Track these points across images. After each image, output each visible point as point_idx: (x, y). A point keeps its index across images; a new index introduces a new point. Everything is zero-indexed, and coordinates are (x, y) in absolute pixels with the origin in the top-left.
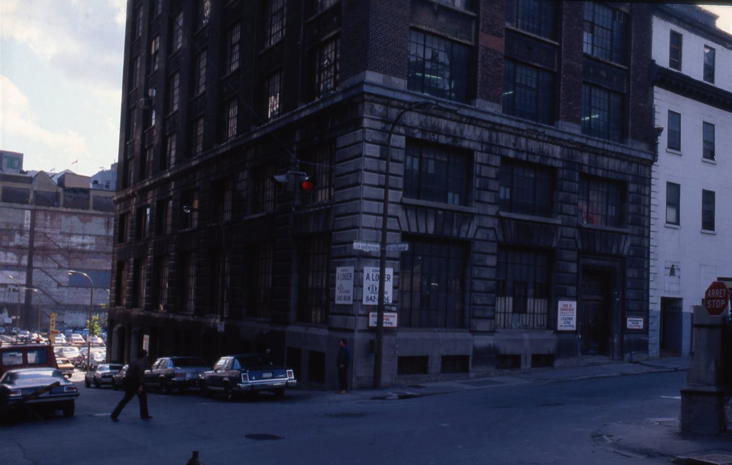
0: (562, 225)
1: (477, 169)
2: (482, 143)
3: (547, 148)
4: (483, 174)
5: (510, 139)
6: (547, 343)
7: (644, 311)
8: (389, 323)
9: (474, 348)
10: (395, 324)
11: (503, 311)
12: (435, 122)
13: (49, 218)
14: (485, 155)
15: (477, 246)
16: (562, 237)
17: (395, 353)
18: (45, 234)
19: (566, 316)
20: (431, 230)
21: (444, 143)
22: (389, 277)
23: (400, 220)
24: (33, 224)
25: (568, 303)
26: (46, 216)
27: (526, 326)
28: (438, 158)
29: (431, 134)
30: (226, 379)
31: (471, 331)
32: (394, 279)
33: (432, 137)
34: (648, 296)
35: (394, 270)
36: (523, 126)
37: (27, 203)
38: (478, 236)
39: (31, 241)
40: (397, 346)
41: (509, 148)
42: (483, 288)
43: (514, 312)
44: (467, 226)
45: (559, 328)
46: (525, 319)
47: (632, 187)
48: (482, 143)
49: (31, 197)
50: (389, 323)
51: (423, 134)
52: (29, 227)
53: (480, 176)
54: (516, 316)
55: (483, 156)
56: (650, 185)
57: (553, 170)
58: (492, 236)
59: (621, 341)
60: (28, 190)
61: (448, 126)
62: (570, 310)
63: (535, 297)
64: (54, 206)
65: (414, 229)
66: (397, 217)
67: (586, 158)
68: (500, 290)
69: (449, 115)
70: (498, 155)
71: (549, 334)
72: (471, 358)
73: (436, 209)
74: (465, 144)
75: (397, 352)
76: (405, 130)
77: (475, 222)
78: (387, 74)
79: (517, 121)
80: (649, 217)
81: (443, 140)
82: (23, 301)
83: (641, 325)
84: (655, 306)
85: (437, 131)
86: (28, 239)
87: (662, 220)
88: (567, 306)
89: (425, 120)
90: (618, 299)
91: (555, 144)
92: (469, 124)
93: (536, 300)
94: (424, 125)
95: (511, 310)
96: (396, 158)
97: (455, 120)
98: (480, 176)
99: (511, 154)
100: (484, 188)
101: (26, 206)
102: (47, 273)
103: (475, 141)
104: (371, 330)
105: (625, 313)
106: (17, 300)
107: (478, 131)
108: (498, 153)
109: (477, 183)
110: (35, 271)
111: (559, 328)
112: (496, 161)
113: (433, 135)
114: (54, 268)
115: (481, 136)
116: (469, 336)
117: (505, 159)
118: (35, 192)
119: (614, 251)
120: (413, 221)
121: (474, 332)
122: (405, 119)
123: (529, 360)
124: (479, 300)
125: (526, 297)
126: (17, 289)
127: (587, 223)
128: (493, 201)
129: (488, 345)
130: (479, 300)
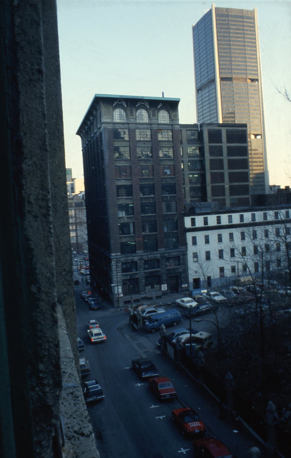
1: (138, 264)
3: (155, 255)
6: (160, 294)
7: (187, 282)
13: (80, 211)
14: (140, 261)
18: (80, 217)
24: (75, 214)
25: (165, 285)
26: (79, 211)
34: (188, 279)
36: (148, 254)
37: (72, 207)
38: (140, 277)
39: (76, 221)
43: (151, 288)
47: (181, 257)
49: (74, 205)
52: (74, 215)
53: (139, 265)
56: (187, 255)
57: (158, 260)
58: (143, 276)
59: (181, 290)
60: (72, 202)
63: (157, 284)
64: (81, 207)
67: (167, 255)
68: (147, 285)
71: (160, 292)
74: (135, 260)
77: (138, 275)
80: (187, 262)
81: (129, 261)
82: (75, 242)
83: (187, 285)
84: (191, 280)
85: (128, 260)
86: (74, 220)
87: (192, 262)
99: (146, 259)
100: (140, 267)
101: (73, 208)
102: (82, 231)
104: (117, 298)
105: (182, 283)
106: (78, 229)
107: (138, 257)
109: (138, 267)
110: (78, 231)
112: (143, 262)
114: (84, 229)
115: (138, 258)
116: (139, 295)
117: (145, 261)
118: (75, 203)
119: (177, 272)
120: (124, 278)
121: (140, 294)
126: (73, 238)
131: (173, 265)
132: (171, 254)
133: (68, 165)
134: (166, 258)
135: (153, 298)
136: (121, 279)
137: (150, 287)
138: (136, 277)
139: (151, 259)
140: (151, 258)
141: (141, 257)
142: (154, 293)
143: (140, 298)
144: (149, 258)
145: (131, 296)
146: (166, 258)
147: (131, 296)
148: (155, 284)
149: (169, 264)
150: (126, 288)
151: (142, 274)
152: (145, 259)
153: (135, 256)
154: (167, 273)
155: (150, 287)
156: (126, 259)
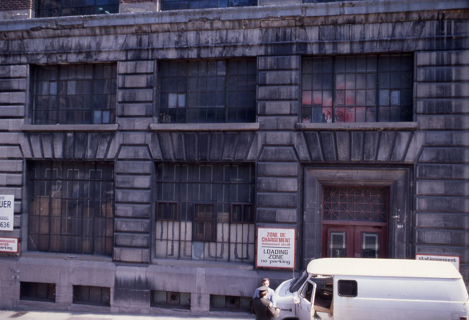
0: (259, 130)
2: (127, 50)
4: (127, 85)
5: (169, 38)
8: (8, 248)
9: (116, 281)
10: (15, 250)
11: (176, 237)
12: (63, 43)
15: (120, 167)
16: (265, 145)
17: (15, 278)
19: (274, 249)
20: (59, 153)
21: (75, 61)
22: (9, 203)
23: (22, 148)
25: (279, 231)
27: (216, 257)
28: (80, 77)
29: (58, 55)
30: (54, 294)
31: (114, 261)
32: (15, 205)
33: (59, 58)
35: (15, 196)
38: (122, 155)
40: (18, 271)
41: (168, 49)
42: (130, 214)
43: (194, 239)
44: (106, 145)
45: (259, 264)
46: (214, 249)
48: (127, 50)
50: (8, 248)
51: (47, 58)
53: (124, 88)
54: (199, 245)
55: (127, 66)
58: (142, 152)
61: (81, 43)
62: (281, 240)
65: (38, 155)
66: (19, 145)
67: (313, 34)
69: (76, 32)
70: (152, 60)
72: (112, 290)
73: (65, 132)
74: (103, 57)
75: (18, 277)
76: (27, 58)
77: (118, 139)
78: (9, 10)
79: (171, 14)
81: (73, 58)
85: (65, 51)
88: (275, 235)
89: (52, 44)
90: (399, 226)
91: (247, 27)
92: (108, 34)
93: (233, 227)
94: (50, 48)
95: (189, 237)
96: (16, 88)
97: (87, 35)
98: (124, 88)
99: (172, 55)
103: (115, 51)
108: (150, 58)
109: (120, 95)
111: (259, 264)
112: (149, 66)
113: (61, 56)
116: (111, 265)
117: (162, 63)
120: (37, 147)
121: (119, 262)
122: (27, 48)
123: (206, 301)
124: (124, 226)
125: (214, 223)
127: (333, 121)
128: (143, 113)
129: (137, 279)
130: (124, 226)
131: (360, 111)
132: (345, 30)
133: (111, 291)
134: (305, 58)
135: (194, 301)
136: (16, 152)
137: (187, 228)
138: (100, 156)
139: (205, 54)
140: (199, 47)
141: (140, 42)
142: (201, 271)
143: (111, 284)
144: (189, 48)
145: (296, 69)
146: (305, 58)
147: (296, 69)
148: (224, 215)
149: (328, 100)
150: (50, 208)
151: (138, 138)
152: (160, 55)
153: (106, 30)
154: (303, 154)
155: (187, 228)
156: (56, 46)
